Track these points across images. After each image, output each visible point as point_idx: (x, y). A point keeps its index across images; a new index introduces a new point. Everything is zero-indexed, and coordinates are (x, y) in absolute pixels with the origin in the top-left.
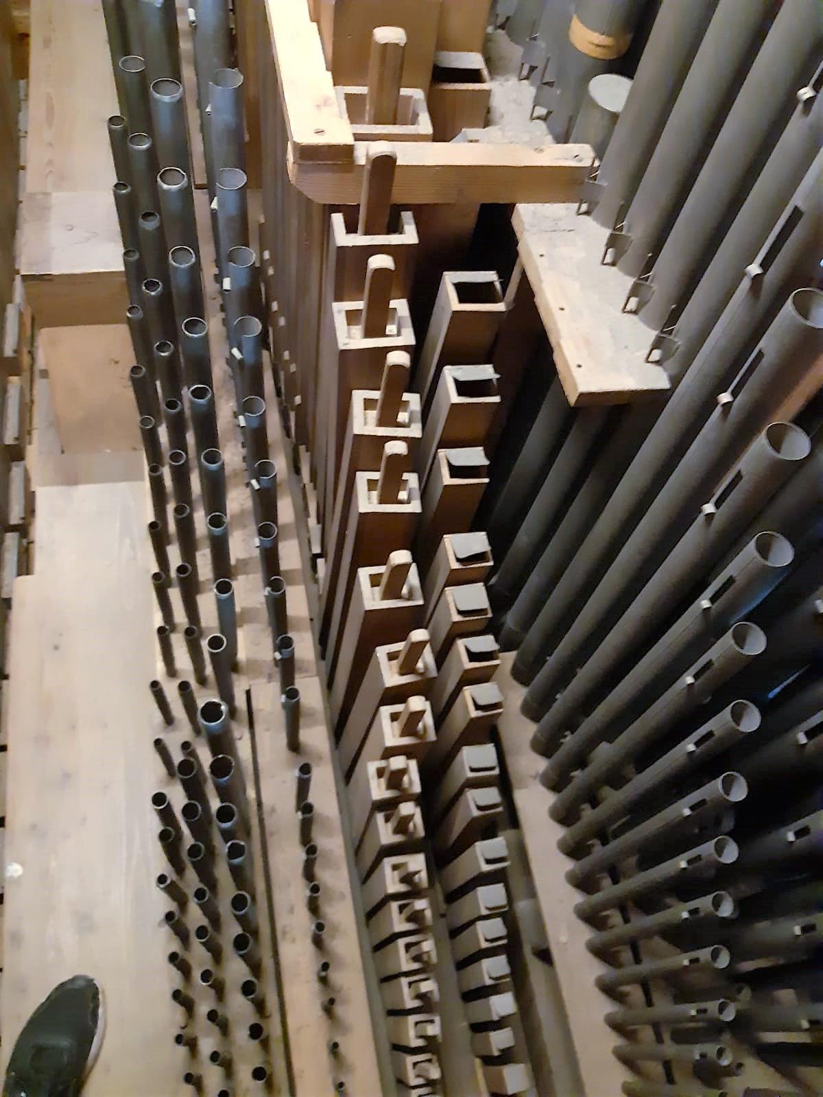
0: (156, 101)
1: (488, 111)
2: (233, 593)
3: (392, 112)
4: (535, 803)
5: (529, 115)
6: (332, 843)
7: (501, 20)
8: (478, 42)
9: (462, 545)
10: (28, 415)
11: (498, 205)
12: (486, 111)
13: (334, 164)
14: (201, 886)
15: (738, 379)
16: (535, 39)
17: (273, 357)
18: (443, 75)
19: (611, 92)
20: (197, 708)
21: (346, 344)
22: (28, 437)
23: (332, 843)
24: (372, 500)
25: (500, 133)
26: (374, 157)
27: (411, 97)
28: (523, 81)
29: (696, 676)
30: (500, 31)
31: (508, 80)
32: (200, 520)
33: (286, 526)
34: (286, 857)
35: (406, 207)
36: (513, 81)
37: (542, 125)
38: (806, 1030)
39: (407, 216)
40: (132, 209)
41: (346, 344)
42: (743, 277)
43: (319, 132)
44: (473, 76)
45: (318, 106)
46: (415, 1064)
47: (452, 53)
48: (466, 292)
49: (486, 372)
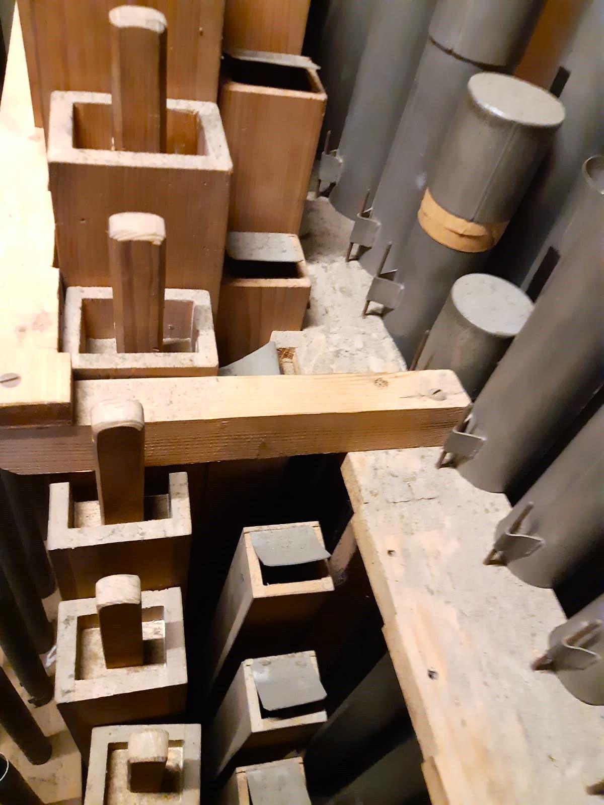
1: (309, 306)
2: (10, 763)
3: (155, 333)
5: (363, 309)
7: (324, 186)
8: (295, 215)
11: (320, 456)
12: (305, 305)
13: (38, 428)
16: (366, 215)
17: (158, 350)
18: (238, 268)
19: (491, 304)
21: (68, 692)
25: (322, 337)
26: (100, 430)
27: (190, 303)
28: (369, 316)
30: (324, 199)
31: (333, 261)
35: (178, 468)
36: (340, 262)
37: (378, 322)
39: (179, 481)
41: (68, 692)
44: (290, 270)
45: (22, 330)
47: (257, 235)
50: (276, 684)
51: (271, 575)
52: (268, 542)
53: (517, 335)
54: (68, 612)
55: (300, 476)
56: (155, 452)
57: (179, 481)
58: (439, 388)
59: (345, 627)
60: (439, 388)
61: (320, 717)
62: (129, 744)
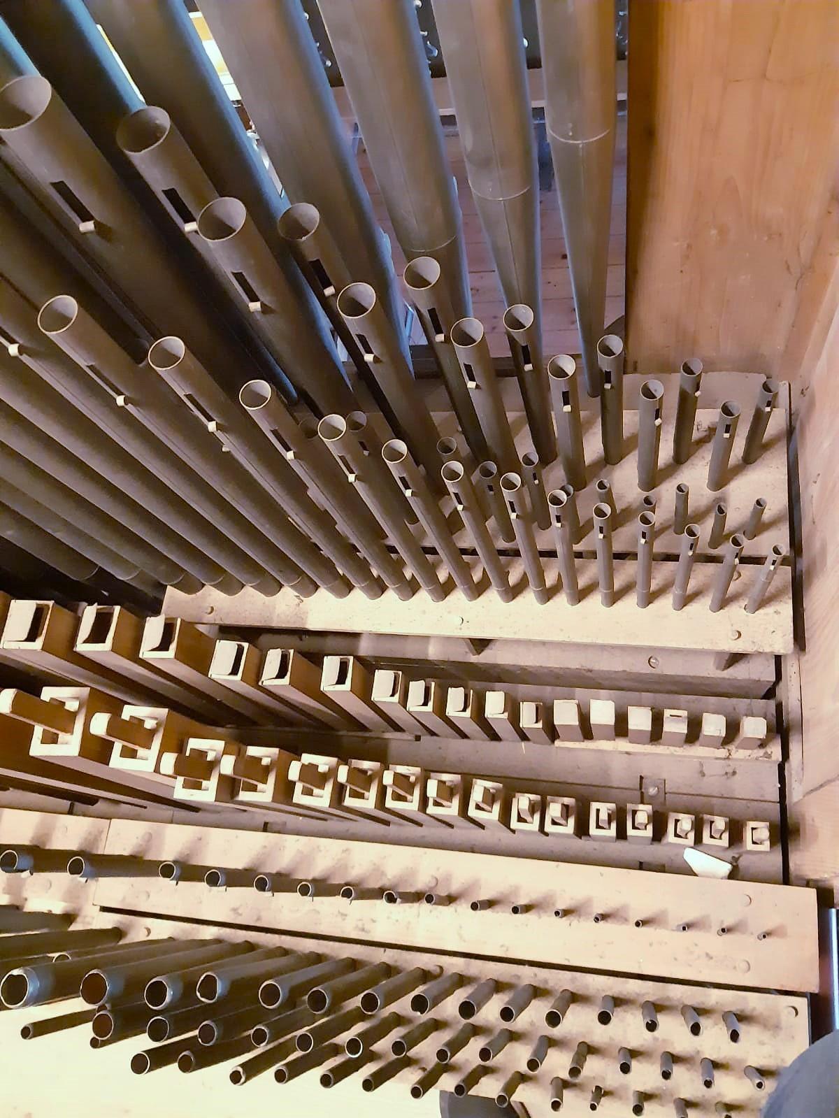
14: (428, 1070)
15: (99, 381)
20: (397, 1059)
24: (321, 795)
29: (288, 449)
34: (288, 910)
38: (771, 410)
41: (192, 795)
46: (598, 827)
48: (98, 635)
49: (89, 614)
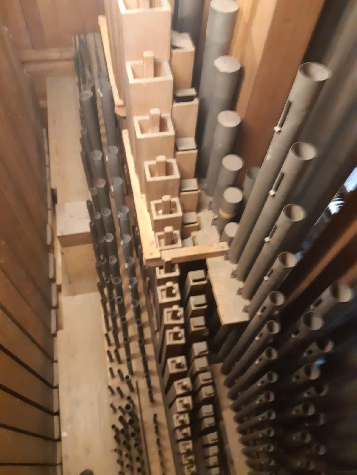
0: (104, 216)
4: (229, 416)
6: (165, 432)
9: (199, 347)
10: (44, 130)
19: (232, 229)
22: (44, 130)
23: (165, 432)
32: (119, 321)
33: (144, 323)
34: (151, 437)
39: (176, 266)
40: (94, 207)
42: (274, 133)
43: (151, 254)
50: (196, 301)
51: (195, 281)
52: (193, 276)
53: (234, 237)
54: (159, 288)
55: (199, 263)
56: (173, 262)
57: (176, 266)
58: (224, 246)
59: (206, 289)
60: (224, 246)
61: (205, 307)
62: (211, 224)
